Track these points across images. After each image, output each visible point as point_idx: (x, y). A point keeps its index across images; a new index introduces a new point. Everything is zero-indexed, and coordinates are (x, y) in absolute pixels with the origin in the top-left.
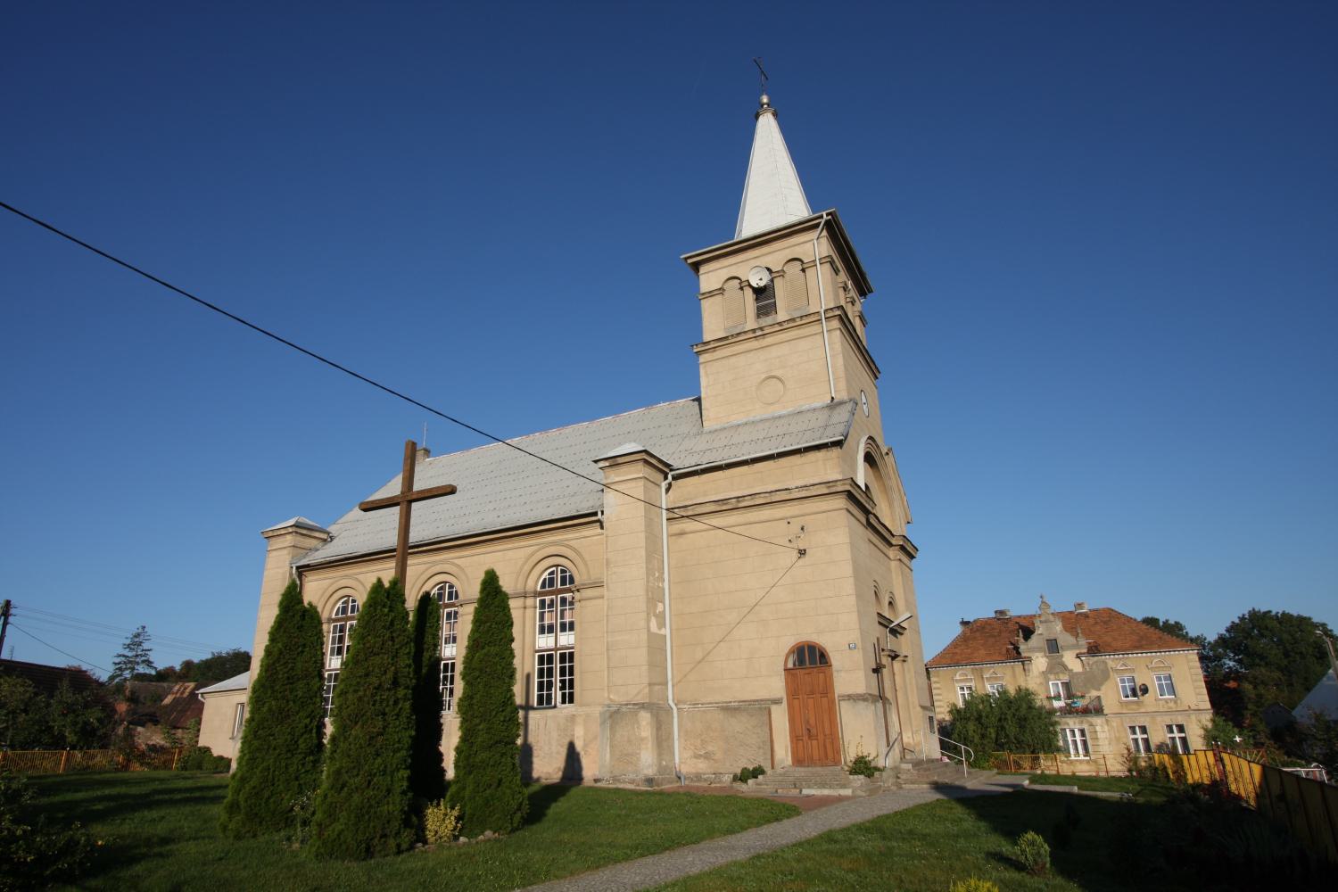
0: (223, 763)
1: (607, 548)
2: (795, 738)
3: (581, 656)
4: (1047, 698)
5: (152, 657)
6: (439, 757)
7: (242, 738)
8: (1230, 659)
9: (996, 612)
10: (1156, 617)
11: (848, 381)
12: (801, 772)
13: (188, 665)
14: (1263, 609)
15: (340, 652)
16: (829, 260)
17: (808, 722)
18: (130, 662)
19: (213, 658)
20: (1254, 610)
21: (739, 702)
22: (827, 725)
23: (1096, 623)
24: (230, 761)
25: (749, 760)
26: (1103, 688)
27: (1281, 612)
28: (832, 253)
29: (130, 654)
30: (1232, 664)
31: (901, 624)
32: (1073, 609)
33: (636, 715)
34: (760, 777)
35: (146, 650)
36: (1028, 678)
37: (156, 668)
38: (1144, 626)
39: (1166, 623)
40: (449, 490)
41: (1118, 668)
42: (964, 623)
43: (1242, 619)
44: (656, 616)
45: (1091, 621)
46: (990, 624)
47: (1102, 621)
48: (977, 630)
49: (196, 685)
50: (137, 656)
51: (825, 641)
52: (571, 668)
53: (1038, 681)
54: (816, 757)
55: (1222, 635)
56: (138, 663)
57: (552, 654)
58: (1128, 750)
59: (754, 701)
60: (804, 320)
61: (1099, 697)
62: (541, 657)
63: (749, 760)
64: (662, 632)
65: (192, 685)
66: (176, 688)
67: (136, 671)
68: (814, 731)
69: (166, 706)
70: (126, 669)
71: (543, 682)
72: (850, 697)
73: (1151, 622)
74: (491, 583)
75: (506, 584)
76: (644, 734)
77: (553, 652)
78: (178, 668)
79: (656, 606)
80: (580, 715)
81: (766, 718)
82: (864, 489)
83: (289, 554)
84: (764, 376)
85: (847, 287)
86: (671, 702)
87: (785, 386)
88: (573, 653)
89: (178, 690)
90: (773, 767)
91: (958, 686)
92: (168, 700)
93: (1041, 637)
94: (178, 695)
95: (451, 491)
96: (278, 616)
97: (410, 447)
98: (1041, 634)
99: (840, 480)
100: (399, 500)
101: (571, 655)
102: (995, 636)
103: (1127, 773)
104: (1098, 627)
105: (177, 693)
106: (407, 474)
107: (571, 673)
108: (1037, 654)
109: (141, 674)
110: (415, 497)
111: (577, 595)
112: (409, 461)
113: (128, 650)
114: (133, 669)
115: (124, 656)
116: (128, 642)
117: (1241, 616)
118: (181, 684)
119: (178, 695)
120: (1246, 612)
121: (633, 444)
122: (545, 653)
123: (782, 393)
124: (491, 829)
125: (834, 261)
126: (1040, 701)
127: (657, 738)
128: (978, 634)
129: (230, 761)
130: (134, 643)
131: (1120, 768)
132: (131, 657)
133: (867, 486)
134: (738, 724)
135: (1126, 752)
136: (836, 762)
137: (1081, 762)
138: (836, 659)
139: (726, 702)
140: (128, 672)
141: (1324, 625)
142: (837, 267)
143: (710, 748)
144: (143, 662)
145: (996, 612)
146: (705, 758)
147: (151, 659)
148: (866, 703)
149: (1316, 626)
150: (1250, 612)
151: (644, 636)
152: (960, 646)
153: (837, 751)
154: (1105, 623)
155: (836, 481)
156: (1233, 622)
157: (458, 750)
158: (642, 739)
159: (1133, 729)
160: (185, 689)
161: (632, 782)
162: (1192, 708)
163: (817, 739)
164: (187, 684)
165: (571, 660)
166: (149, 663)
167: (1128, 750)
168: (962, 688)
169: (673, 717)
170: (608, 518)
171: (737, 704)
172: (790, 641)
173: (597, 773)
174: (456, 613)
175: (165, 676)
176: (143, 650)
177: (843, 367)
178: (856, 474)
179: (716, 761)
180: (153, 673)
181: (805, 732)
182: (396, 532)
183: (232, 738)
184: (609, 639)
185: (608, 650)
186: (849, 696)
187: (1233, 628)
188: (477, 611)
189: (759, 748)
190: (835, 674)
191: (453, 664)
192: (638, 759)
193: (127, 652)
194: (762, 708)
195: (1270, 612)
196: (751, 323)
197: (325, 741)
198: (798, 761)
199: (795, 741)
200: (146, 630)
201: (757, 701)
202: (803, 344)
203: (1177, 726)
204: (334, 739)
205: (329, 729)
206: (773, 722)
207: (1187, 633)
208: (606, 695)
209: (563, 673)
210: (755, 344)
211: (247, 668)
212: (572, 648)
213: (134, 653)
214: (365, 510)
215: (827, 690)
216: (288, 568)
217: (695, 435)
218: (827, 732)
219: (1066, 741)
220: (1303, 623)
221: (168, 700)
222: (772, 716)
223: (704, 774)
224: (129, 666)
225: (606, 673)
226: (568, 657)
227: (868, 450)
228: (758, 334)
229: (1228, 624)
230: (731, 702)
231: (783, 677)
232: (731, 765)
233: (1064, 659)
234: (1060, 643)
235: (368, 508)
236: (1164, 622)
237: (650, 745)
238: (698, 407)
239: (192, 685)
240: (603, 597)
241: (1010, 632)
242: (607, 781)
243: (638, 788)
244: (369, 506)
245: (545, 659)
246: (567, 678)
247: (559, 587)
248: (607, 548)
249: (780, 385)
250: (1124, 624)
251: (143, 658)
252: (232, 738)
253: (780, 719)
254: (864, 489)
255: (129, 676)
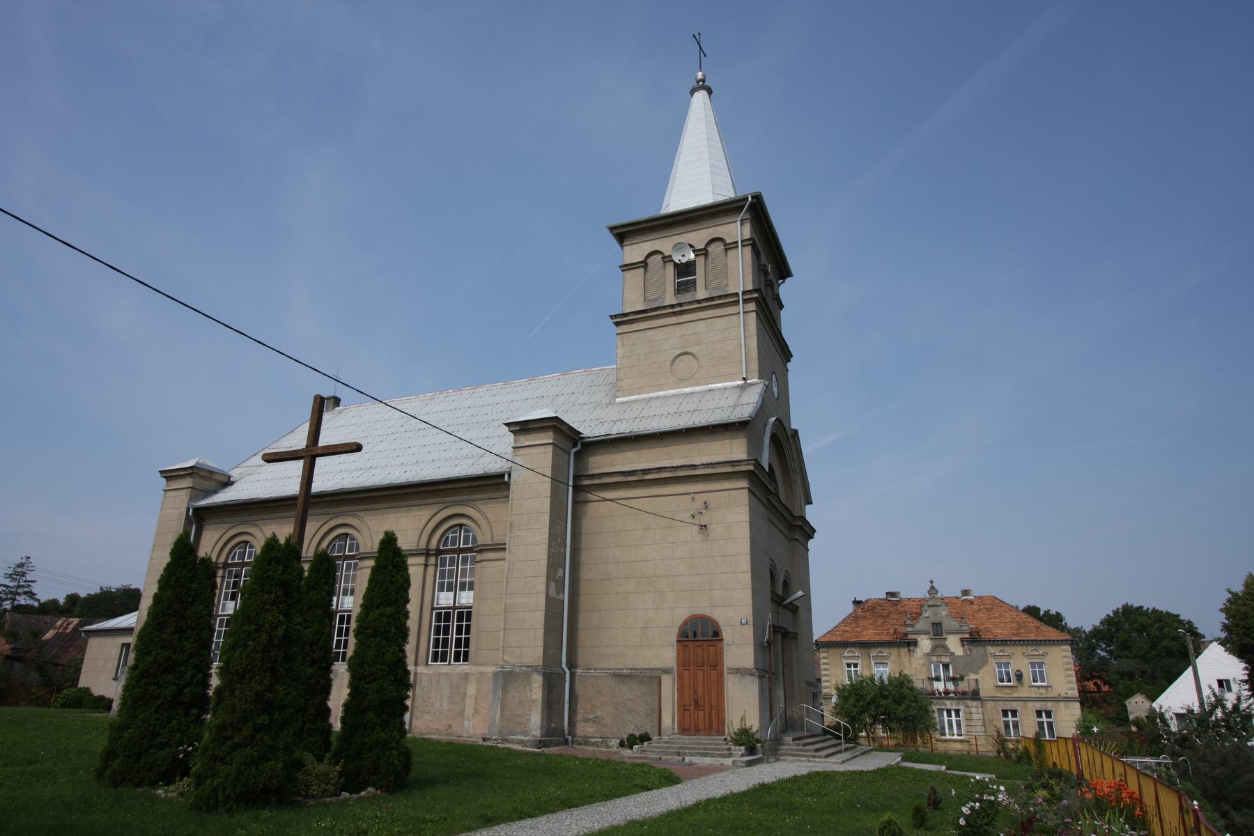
0: (103, 703)
1: (511, 511)
2: (683, 708)
3: (478, 616)
4: (929, 678)
5: (35, 588)
6: (327, 711)
7: (123, 686)
8: (1102, 650)
9: (887, 593)
10: (1038, 606)
11: (760, 363)
12: (686, 740)
13: (73, 599)
14: (1136, 605)
15: (233, 597)
16: (751, 242)
17: (695, 692)
18: (11, 593)
19: (101, 594)
20: (1127, 604)
21: (631, 669)
22: (714, 694)
23: (980, 610)
24: (111, 701)
25: (637, 726)
26: (981, 672)
27: (1151, 608)
28: (755, 237)
29: (12, 584)
30: (1103, 654)
31: (794, 602)
32: (959, 595)
33: (529, 677)
34: (646, 743)
35: (29, 581)
36: (912, 659)
37: (39, 600)
38: (1024, 616)
39: (1047, 613)
40: (354, 447)
41: (997, 654)
42: (856, 603)
43: (1116, 612)
44: (556, 581)
45: (976, 607)
46: (880, 605)
47: (985, 608)
48: (868, 610)
49: (80, 621)
50: (19, 586)
51: (719, 615)
52: (468, 627)
53: (921, 662)
54: (701, 726)
55: (1096, 626)
56: (19, 594)
57: (450, 612)
58: (998, 732)
59: (646, 669)
60: (723, 301)
61: (977, 680)
62: (439, 615)
63: (637, 726)
64: (560, 597)
65: (76, 621)
66: (59, 623)
67: (16, 603)
68: (701, 702)
69: (48, 641)
70: (7, 599)
71: (441, 625)
72: (738, 671)
73: (1032, 611)
74: (389, 541)
75: (404, 543)
76: (534, 696)
77: (452, 611)
78: (62, 600)
79: (556, 571)
80: (473, 674)
81: (656, 687)
82: (767, 469)
83: (186, 495)
84: (679, 352)
85: (767, 270)
86: (564, 666)
87: (698, 363)
88: (471, 612)
89: (61, 626)
90: (660, 734)
91: (845, 661)
92: (50, 635)
93: (927, 620)
94: (61, 631)
95: (357, 448)
96: (168, 564)
97: (318, 400)
98: (928, 618)
99: (745, 461)
100: (303, 454)
101: (469, 614)
102: (883, 617)
103: (995, 754)
104: (981, 614)
105: (59, 628)
106: (314, 428)
107: (468, 632)
108: (923, 636)
109: (22, 605)
110: (319, 452)
111: (479, 557)
112: (316, 416)
113: (10, 579)
114: (14, 599)
115: (4, 586)
116: (10, 571)
117: (1115, 609)
118: (65, 619)
119: (61, 631)
120: (1120, 607)
121: (546, 410)
122: (443, 611)
123: (695, 370)
124: (373, 786)
125: (756, 245)
126: (919, 684)
127: (548, 701)
128: (868, 613)
129: (111, 701)
130: (16, 573)
131: (990, 748)
132: (13, 588)
133: (770, 466)
134: (629, 692)
135: (996, 734)
136: (720, 732)
137: (955, 741)
138: (727, 635)
139: (619, 669)
140: (9, 602)
141: (1189, 622)
142: (758, 250)
143: (599, 713)
144: (25, 593)
145: (887, 593)
146: (594, 722)
147: (34, 591)
148: (752, 678)
149: (1181, 623)
150: (1124, 605)
151: (543, 601)
152: (851, 624)
153: (722, 722)
154: (988, 610)
155: (741, 461)
156: (1108, 615)
157: (347, 706)
158: (533, 701)
159: (1005, 713)
160: (68, 624)
161: (521, 742)
162: (1062, 695)
163: (704, 710)
164: (71, 620)
165: (469, 619)
166: (31, 595)
167: (998, 732)
168: (849, 665)
169: (565, 682)
170: (515, 481)
171: (628, 671)
172: (683, 614)
173: (487, 732)
174: (356, 565)
175: (51, 608)
176: (26, 581)
177: (756, 349)
178: (761, 456)
179: (604, 726)
180: (36, 604)
181: (692, 702)
182: (299, 480)
183: (116, 679)
184: (508, 601)
185: (505, 612)
186: (737, 669)
187: (1108, 621)
188: (375, 570)
189: (647, 715)
190: (725, 648)
191: (349, 617)
192: (528, 720)
193: (8, 582)
194: (652, 678)
195: (1142, 607)
196: (670, 299)
197: (211, 693)
198: (683, 730)
199: (682, 710)
200: (30, 561)
201: (649, 669)
202: (721, 323)
203: (1046, 711)
204: (218, 691)
205: (215, 682)
206: (662, 692)
207: (1066, 624)
208: (501, 656)
209: (459, 631)
210: (673, 320)
211: (135, 608)
212: (471, 607)
213: (16, 584)
214: (268, 461)
215: (716, 664)
216: (184, 510)
217: (607, 405)
218: (714, 703)
219: (942, 722)
220: (1173, 619)
221: (50, 635)
222: (663, 685)
223: (592, 738)
224: (10, 596)
225: (502, 635)
226: (465, 615)
227: (776, 431)
228: (676, 310)
229: (1103, 616)
230: (623, 669)
231: (675, 647)
232: (619, 731)
233: (946, 643)
234: (945, 627)
235: (271, 459)
236: (1045, 612)
237: (540, 707)
238: (593, 503)
239: (76, 621)
240: (504, 559)
241: (899, 614)
242: (495, 740)
243: (524, 748)
244: (272, 458)
245: (443, 615)
246: (463, 636)
247: (461, 546)
248: (511, 511)
249: (694, 362)
250: (1006, 612)
251: (26, 589)
252: (116, 679)
253: (669, 688)
254: (767, 469)
255: (8, 607)
